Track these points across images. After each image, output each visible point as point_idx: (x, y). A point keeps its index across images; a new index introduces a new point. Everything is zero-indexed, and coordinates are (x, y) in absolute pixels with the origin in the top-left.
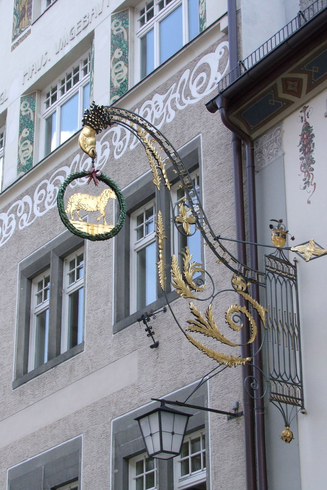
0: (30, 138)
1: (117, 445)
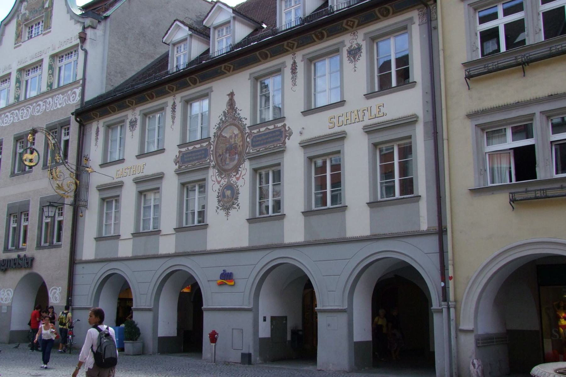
0: (19, 87)
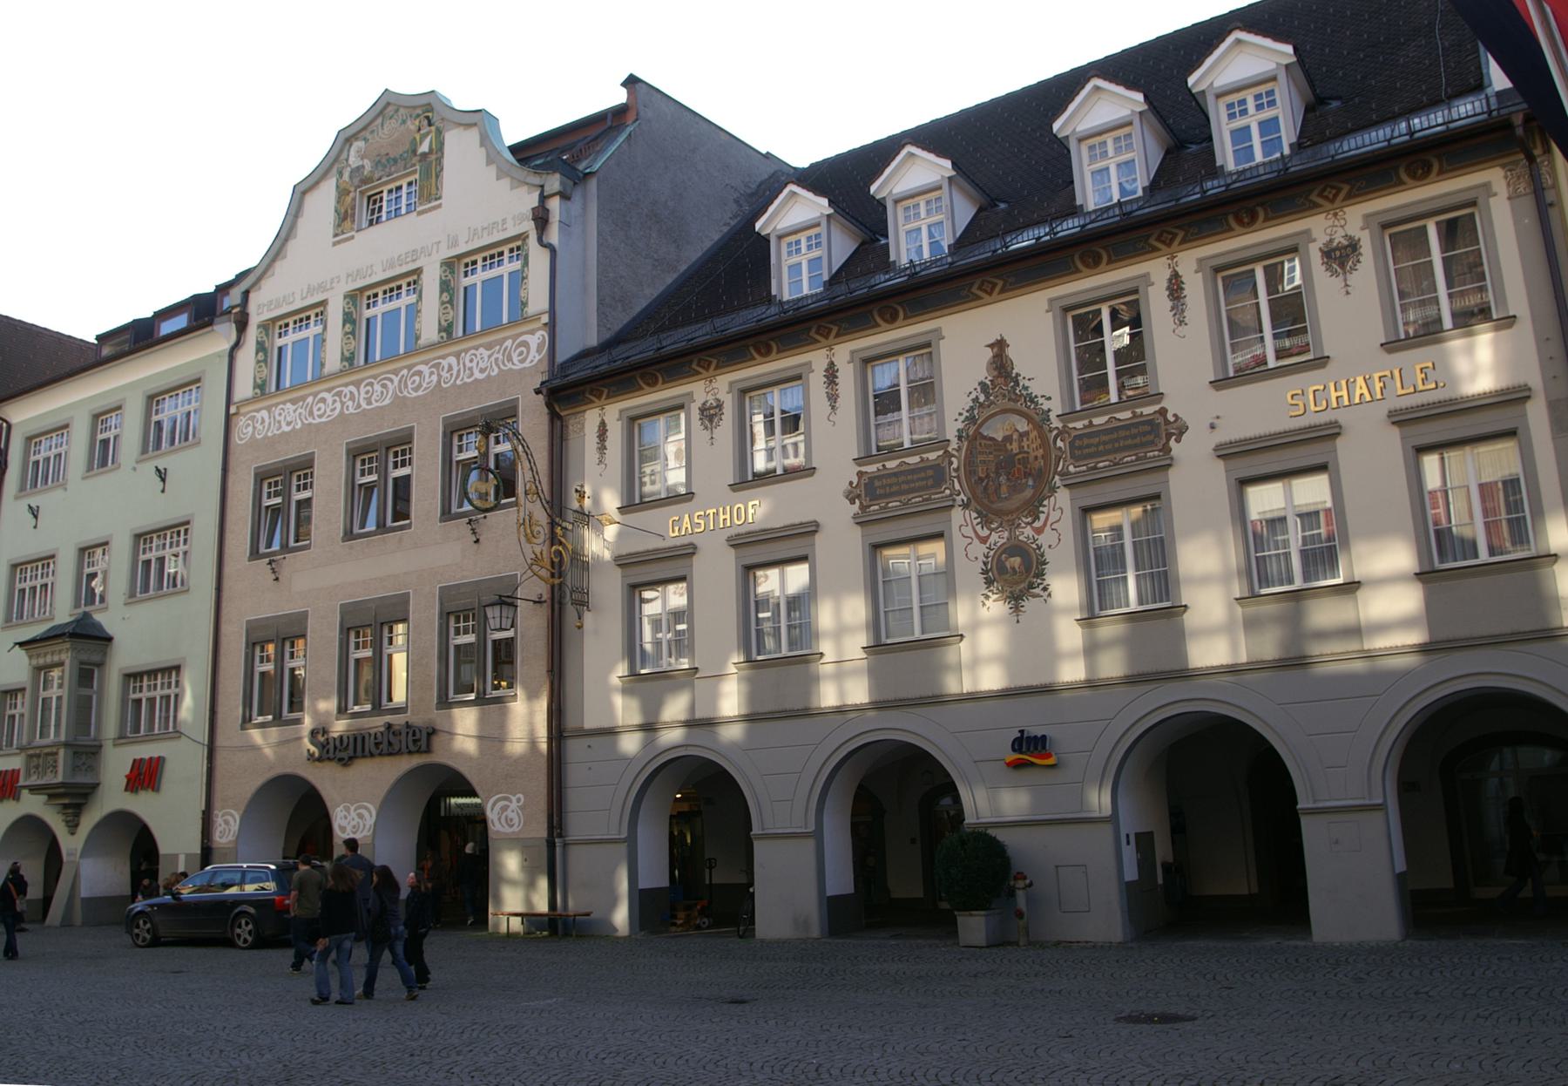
1: (441, 604)
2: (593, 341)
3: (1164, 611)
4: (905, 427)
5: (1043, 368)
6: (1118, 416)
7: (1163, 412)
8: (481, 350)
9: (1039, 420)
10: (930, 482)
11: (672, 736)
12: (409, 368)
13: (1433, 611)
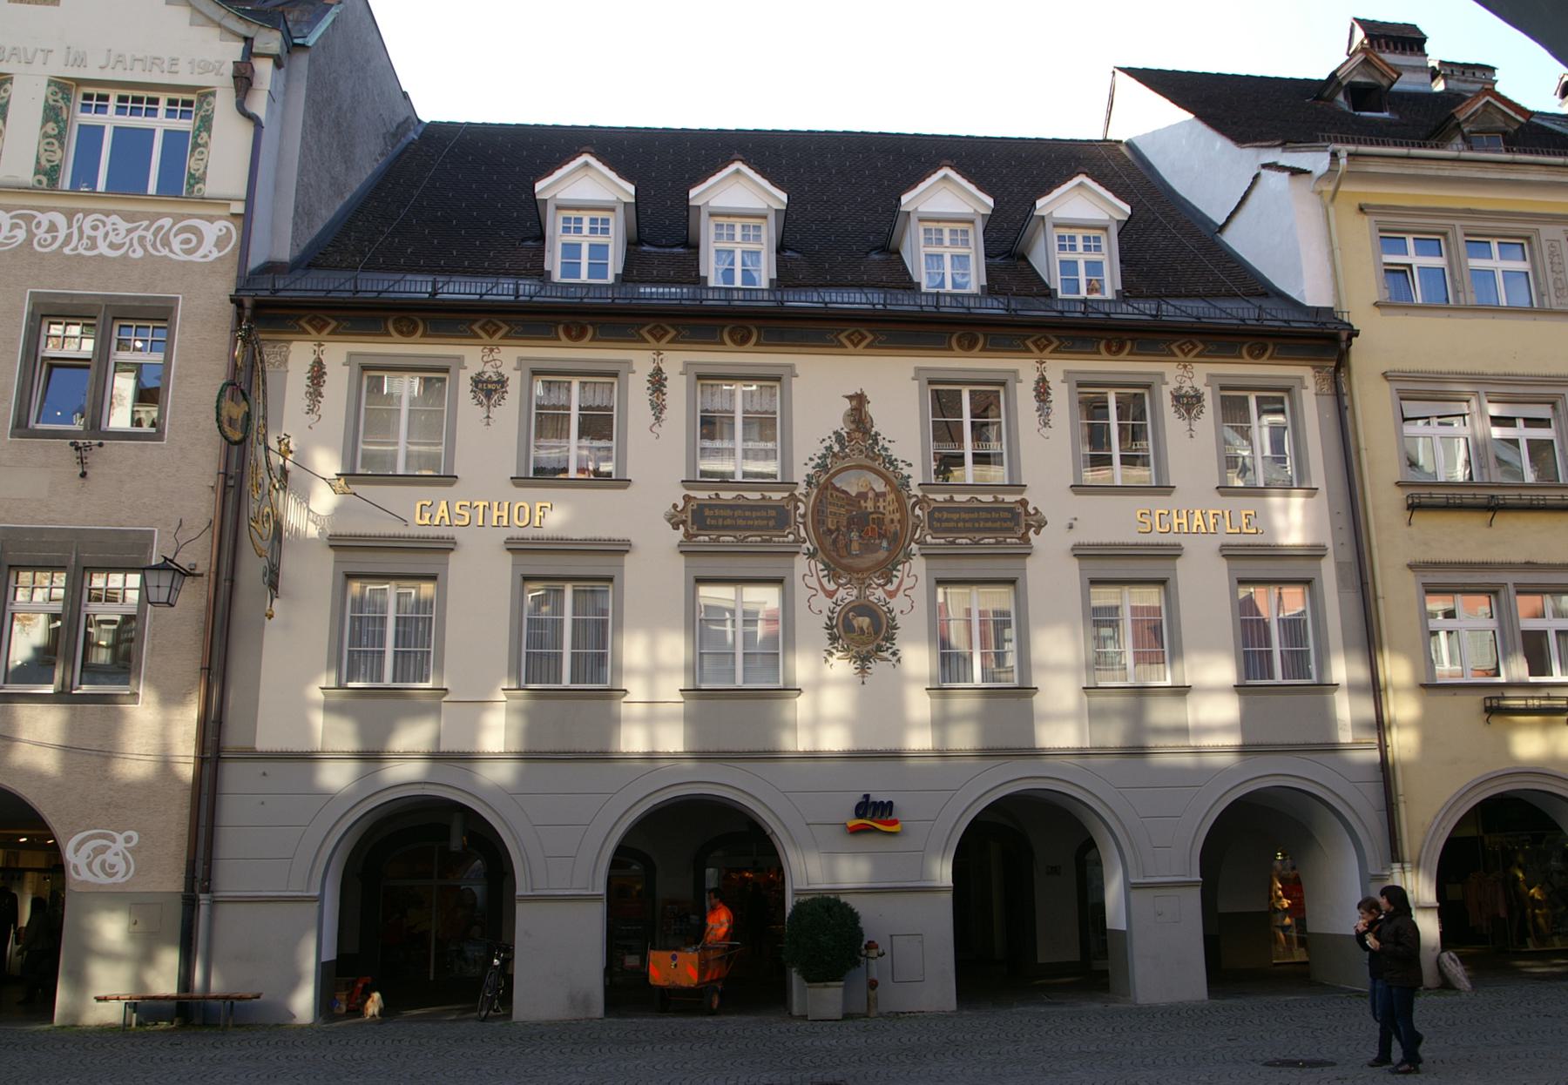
2: (285, 254)
3: (1015, 695)
4: (736, 460)
5: (904, 430)
6: (980, 497)
7: (1024, 503)
8: (114, 218)
9: (899, 485)
10: (772, 523)
11: (404, 772)
12: (178, 218)
13: (1246, 722)
